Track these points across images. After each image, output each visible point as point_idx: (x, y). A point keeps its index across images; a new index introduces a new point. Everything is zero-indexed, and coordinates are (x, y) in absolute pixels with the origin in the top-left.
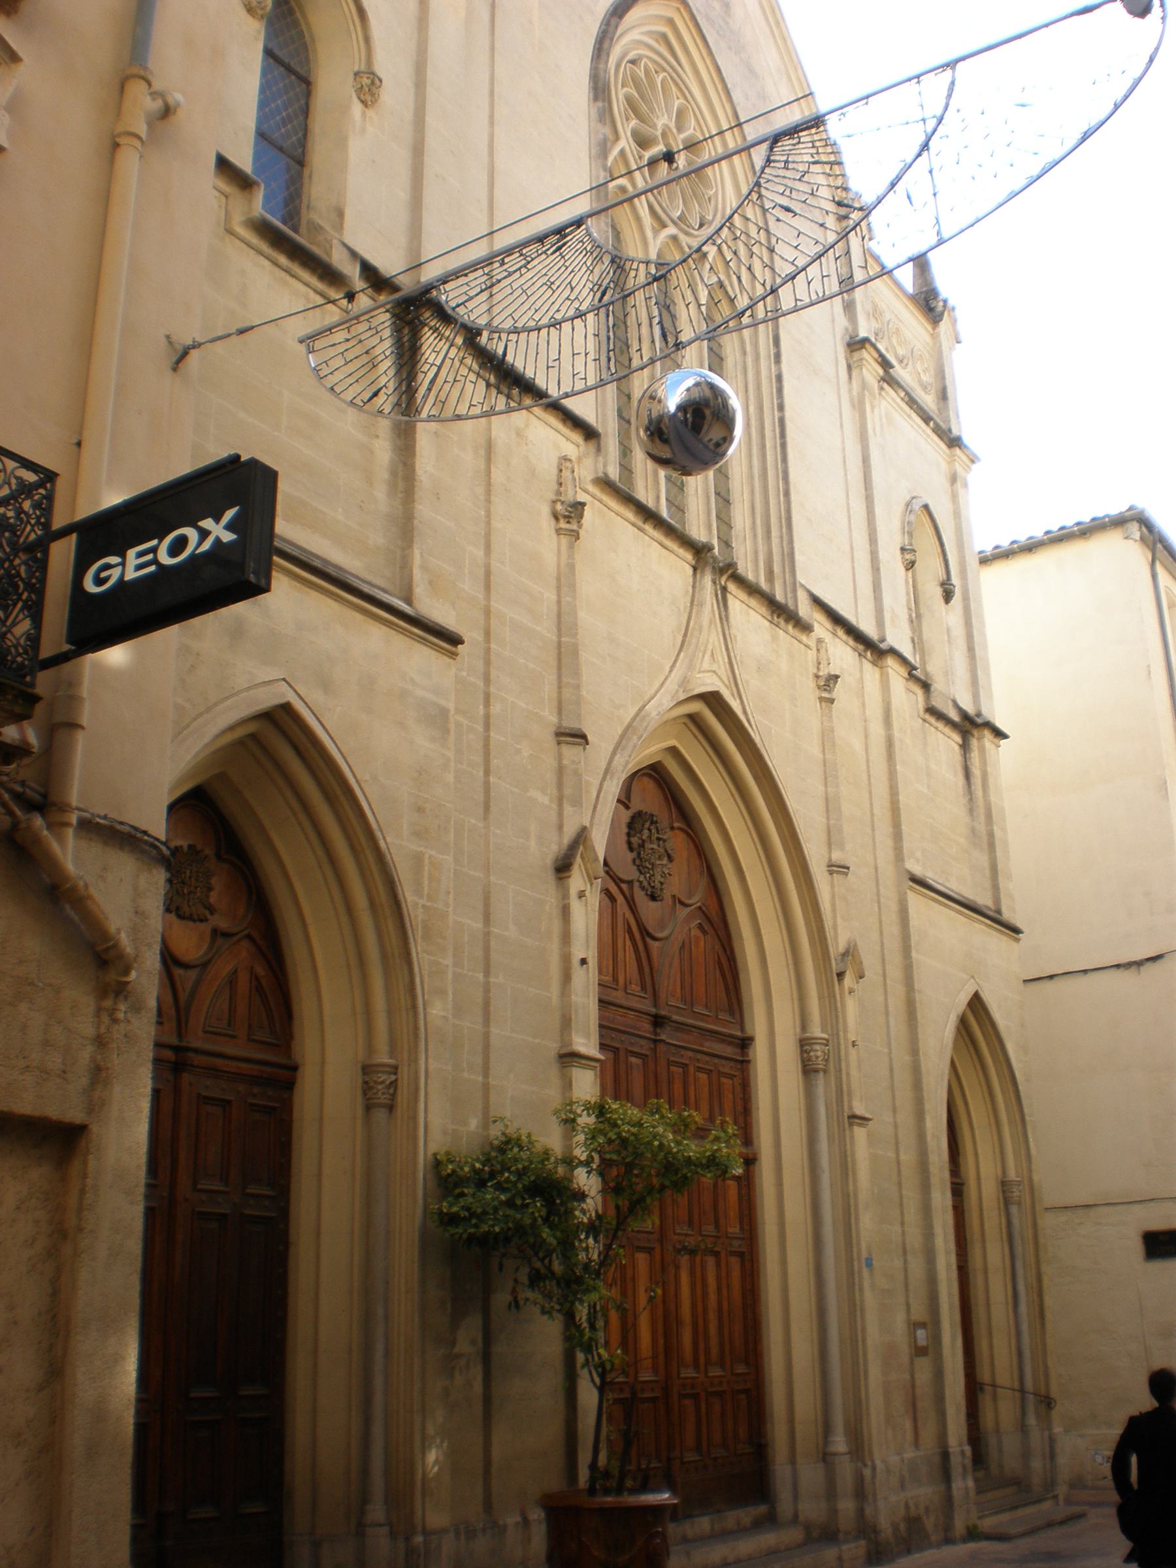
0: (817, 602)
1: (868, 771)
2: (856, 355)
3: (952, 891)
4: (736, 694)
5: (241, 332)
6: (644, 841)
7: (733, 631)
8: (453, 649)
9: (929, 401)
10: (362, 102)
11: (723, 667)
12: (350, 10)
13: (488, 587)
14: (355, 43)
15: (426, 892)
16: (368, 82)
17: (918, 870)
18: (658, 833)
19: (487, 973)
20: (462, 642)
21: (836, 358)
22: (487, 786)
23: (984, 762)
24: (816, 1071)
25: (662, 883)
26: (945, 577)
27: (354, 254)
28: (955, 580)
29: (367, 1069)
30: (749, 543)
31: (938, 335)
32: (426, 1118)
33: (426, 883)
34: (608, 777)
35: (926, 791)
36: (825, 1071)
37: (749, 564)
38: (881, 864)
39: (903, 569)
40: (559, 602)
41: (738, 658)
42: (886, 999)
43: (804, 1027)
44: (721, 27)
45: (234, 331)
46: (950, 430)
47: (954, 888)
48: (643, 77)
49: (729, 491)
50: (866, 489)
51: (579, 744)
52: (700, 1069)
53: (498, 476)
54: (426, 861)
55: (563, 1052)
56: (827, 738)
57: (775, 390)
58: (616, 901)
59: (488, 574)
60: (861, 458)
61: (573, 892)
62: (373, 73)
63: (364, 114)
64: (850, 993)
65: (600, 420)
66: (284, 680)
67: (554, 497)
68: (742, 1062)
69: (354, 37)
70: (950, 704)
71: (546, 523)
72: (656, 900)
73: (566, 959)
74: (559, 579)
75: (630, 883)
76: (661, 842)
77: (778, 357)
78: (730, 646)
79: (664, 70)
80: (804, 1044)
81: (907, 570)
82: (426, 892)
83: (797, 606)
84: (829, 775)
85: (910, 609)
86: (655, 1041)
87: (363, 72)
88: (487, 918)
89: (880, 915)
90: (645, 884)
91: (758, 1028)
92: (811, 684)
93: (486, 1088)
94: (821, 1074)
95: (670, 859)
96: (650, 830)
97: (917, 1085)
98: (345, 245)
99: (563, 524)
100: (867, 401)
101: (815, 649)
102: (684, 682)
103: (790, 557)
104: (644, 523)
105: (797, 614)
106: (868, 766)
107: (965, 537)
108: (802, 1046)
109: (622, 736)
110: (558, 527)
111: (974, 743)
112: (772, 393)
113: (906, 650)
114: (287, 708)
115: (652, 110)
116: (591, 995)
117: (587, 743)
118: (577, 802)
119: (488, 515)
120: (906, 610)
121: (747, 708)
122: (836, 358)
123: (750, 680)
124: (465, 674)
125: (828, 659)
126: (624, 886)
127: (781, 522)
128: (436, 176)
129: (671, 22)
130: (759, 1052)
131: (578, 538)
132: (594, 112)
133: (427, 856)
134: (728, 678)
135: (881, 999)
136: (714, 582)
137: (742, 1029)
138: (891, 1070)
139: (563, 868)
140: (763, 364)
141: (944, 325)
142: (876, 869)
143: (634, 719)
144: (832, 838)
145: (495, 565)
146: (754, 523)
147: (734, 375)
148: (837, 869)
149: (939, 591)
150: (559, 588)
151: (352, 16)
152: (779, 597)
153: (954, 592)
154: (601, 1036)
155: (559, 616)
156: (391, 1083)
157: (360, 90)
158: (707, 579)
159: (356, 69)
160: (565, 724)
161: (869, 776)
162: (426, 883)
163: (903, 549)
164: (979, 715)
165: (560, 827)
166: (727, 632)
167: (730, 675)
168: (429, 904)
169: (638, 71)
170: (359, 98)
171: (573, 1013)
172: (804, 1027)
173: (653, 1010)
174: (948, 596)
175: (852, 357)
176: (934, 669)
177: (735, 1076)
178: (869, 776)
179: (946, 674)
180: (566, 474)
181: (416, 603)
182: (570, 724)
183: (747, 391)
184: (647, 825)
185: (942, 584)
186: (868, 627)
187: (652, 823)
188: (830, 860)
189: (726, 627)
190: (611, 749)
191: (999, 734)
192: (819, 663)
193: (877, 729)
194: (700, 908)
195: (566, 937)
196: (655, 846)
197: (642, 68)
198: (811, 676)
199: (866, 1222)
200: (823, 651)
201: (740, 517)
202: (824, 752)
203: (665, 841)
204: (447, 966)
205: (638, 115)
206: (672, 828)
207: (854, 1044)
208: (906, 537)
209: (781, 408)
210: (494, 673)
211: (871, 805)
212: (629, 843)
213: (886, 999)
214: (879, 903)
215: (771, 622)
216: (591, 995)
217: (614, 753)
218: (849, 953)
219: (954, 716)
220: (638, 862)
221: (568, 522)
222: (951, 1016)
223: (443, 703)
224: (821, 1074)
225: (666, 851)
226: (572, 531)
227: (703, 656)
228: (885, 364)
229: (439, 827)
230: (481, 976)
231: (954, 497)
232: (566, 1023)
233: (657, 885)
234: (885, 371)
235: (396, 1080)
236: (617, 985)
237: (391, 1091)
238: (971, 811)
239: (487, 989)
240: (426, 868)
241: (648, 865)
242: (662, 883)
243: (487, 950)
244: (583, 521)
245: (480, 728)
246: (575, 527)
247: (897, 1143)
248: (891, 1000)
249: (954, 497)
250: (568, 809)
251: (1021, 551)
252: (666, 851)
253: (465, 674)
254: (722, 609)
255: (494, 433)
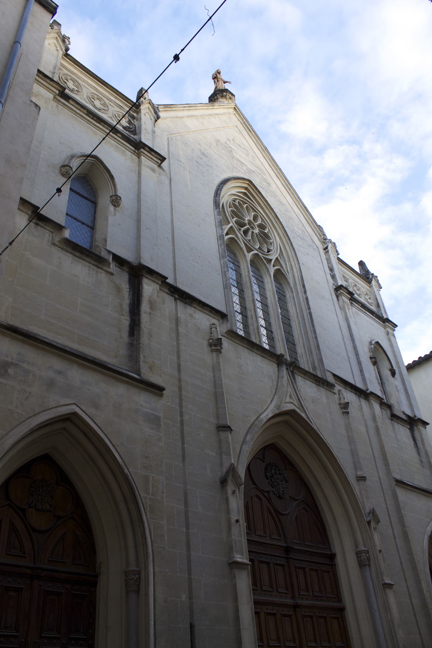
0: (335, 375)
1: (370, 440)
2: (339, 292)
3: (416, 485)
4: (303, 411)
5: (11, 244)
6: (272, 474)
7: (299, 388)
8: (161, 392)
9: (373, 308)
10: (114, 205)
11: (295, 401)
12: (108, 178)
13: (179, 371)
14: (110, 188)
15: (151, 492)
16: (115, 198)
17: (398, 477)
18: (279, 470)
19: (187, 528)
20: (164, 389)
21: (331, 293)
22: (183, 449)
23: (421, 435)
24: (365, 565)
25: (283, 491)
26: (391, 367)
27: (109, 252)
28: (395, 368)
29: (126, 573)
30: (304, 357)
31: (372, 286)
32: (154, 595)
33: (151, 488)
34: (244, 444)
35: (397, 446)
36: (369, 565)
37: (305, 365)
38: (381, 476)
39: (372, 366)
40: (214, 376)
41: (303, 398)
42: (393, 532)
43: (357, 547)
44: (266, 190)
45: (8, 245)
46: (383, 317)
47: (417, 484)
48: (238, 205)
49: (294, 340)
50: (351, 337)
51: (228, 431)
52: (311, 570)
53: (182, 330)
54: (151, 479)
55: (230, 562)
56: (348, 428)
57: (306, 303)
58: (262, 499)
59: (179, 366)
60: (347, 326)
61: (230, 491)
62: (117, 195)
63: (115, 209)
64: (374, 529)
65: (228, 312)
66: (75, 404)
67: (209, 338)
68: (332, 565)
69: (110, 188)
70: (402, 413)
71: (206, 348)
72: (282, 499)
73: (229, 520)
74: (213, 368)
75: (268, 492)
76: (281, 475)
77: (305, 292)
78: (298, 392)
79: (246, 203)
80: (358, 554)
81: (374, 365)
82: (151, 492)
83: (326, 378)
84: (351, 441)
85: (378, 379)
86: (288, 558)
87: (113, 196)
88: (186, 503)
89: (384, 497)
90: (276, 492)
91: (337, 549)
92: (338, 407)
93: (190, 581)
94: (367, 567)
95: (286, 481)
96: (275, 470)
97: (414, 568)
98: (106, 249)
99: (213, 348)
100: (346, 307)
101: (337, 394)
102: (278, 407)
103: (321, 360)
104: (252, 348)
105: (327, 381)
106: (369, 438)
107: (396, 353)
108: (357, 555)
109: (249, 428)
110: (211, 349)
111: (415, 428)
112: (305, 304)
113: (379, 394)
114: (75, 414)
115: (243, 215)
116: (243, 535)
117: (232, 430)
118: (228, 454)
119: (178, 344)
120: (376, 380)
121: (309, 416)
122: (331, 293)
123: (307, 404)
124: (170, 404)
125: (344, 397)
126: (266, 494)
127: (315, 348)
128: (147, 228)
129: (246, 188)
130: (339, 560)
131: (221, 353)
132: (216, 212)
133: (151, 477)
134: (299, 405)
135: (391, 531)
136: (287, 369)
137: (330, 550)
138: (401, 562)
139: (223, 482)
140: (300, 295)
141: (374, 282)
142: (380, 478)
143: (255, 421)
144: (356, 466)
145: (182, 363)
146: (305, 350)
147: (290, 301)
148: (362, 479)
149: (389, 373)
150: (214, 371)
151: (108, 179)
152: (319, 375)
153: (395, 372)
154: (250, 555)
155: (215, 381)
156: (137, 579)
157: (112, 202)
158: (284, 368)
159: (111, 195)
160: (220, 423)
161: (370, 442)
162: (151, 488)
163: (371, 358)
164: (415, 416)
165: (221, 465)
166: (296, 387)
167: (299, 403)
168: (152, 497)
169: (236, 204)
170: (112, 204)
171: (233, 543)
172: (357, 547)
173: (285, 545)
174: (393, 373)
175: (337, 293)
176: (393, 401)
177: (330, 571)
178: (370, 442)
179: (398, 403)
180: (213, 329)
181: (142, 375)
182: (222, 422)
183: (295, 305)
184: (274, 468)
185: (390, 370)
186: (360, 385)
187: (276, 467)
188: (357, 475)
189: (295, 386)
190: (245, 433)
191: (425, 424)
192: (340, 399)
193: (370, 423)
194: (303, 501)
195: (228, 511)
196: (278, 476)
197: (237, 203)
198: (337, 404)
199: (400, 634)
200: (341, 395)
201: (300, 349)
202: (347, 433)
203: (283, 474)
204: (164, 524)
205: (237, 216)
206: (286, 469)
207: (380, 551)
208: (371, 353)
209: (309, 308)
210: (184, 404)
211: (373, 453)
212: (266, 476)
213: (393, 532)
214: (383, 492)
215: (316, 384)
216: (243, 535)
217: (246, 435)
218: (373, 512)
219: (404, 417)
220: (271, 483)
221: (216, 347)
222: (425, 537)
223: (157, 414)
224: (367, 567)
225: (284, 478)
226: (217, 349)
227: (286, 397)
228: (351, 294)
229: (157, 465)
230: (184, 529)
231: (389, 340)
232: (231, 549)
233: (281, 492)
234: (351, 296)
235: (140, 577)
236: (266, 535)
237: (138, 583)
238: (419, 454)
239: (188, 535)
240: (151, 482)
241: (275, 484)
242: (283, 491)
243: (187, 517)
244: (223, 346)
245: (179, 425)
246: (219, 348)
247: (410, 595)
248: (395, 532)
249: (389, 340)
250: (224, 457)
251: (423, 361)
252: (284, 478)
253: (170, 404)
254: (292, 379)
255: (179, 315)
